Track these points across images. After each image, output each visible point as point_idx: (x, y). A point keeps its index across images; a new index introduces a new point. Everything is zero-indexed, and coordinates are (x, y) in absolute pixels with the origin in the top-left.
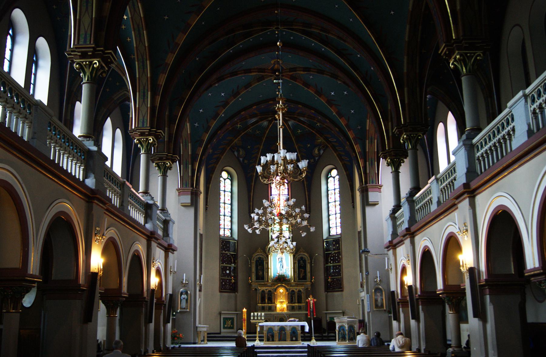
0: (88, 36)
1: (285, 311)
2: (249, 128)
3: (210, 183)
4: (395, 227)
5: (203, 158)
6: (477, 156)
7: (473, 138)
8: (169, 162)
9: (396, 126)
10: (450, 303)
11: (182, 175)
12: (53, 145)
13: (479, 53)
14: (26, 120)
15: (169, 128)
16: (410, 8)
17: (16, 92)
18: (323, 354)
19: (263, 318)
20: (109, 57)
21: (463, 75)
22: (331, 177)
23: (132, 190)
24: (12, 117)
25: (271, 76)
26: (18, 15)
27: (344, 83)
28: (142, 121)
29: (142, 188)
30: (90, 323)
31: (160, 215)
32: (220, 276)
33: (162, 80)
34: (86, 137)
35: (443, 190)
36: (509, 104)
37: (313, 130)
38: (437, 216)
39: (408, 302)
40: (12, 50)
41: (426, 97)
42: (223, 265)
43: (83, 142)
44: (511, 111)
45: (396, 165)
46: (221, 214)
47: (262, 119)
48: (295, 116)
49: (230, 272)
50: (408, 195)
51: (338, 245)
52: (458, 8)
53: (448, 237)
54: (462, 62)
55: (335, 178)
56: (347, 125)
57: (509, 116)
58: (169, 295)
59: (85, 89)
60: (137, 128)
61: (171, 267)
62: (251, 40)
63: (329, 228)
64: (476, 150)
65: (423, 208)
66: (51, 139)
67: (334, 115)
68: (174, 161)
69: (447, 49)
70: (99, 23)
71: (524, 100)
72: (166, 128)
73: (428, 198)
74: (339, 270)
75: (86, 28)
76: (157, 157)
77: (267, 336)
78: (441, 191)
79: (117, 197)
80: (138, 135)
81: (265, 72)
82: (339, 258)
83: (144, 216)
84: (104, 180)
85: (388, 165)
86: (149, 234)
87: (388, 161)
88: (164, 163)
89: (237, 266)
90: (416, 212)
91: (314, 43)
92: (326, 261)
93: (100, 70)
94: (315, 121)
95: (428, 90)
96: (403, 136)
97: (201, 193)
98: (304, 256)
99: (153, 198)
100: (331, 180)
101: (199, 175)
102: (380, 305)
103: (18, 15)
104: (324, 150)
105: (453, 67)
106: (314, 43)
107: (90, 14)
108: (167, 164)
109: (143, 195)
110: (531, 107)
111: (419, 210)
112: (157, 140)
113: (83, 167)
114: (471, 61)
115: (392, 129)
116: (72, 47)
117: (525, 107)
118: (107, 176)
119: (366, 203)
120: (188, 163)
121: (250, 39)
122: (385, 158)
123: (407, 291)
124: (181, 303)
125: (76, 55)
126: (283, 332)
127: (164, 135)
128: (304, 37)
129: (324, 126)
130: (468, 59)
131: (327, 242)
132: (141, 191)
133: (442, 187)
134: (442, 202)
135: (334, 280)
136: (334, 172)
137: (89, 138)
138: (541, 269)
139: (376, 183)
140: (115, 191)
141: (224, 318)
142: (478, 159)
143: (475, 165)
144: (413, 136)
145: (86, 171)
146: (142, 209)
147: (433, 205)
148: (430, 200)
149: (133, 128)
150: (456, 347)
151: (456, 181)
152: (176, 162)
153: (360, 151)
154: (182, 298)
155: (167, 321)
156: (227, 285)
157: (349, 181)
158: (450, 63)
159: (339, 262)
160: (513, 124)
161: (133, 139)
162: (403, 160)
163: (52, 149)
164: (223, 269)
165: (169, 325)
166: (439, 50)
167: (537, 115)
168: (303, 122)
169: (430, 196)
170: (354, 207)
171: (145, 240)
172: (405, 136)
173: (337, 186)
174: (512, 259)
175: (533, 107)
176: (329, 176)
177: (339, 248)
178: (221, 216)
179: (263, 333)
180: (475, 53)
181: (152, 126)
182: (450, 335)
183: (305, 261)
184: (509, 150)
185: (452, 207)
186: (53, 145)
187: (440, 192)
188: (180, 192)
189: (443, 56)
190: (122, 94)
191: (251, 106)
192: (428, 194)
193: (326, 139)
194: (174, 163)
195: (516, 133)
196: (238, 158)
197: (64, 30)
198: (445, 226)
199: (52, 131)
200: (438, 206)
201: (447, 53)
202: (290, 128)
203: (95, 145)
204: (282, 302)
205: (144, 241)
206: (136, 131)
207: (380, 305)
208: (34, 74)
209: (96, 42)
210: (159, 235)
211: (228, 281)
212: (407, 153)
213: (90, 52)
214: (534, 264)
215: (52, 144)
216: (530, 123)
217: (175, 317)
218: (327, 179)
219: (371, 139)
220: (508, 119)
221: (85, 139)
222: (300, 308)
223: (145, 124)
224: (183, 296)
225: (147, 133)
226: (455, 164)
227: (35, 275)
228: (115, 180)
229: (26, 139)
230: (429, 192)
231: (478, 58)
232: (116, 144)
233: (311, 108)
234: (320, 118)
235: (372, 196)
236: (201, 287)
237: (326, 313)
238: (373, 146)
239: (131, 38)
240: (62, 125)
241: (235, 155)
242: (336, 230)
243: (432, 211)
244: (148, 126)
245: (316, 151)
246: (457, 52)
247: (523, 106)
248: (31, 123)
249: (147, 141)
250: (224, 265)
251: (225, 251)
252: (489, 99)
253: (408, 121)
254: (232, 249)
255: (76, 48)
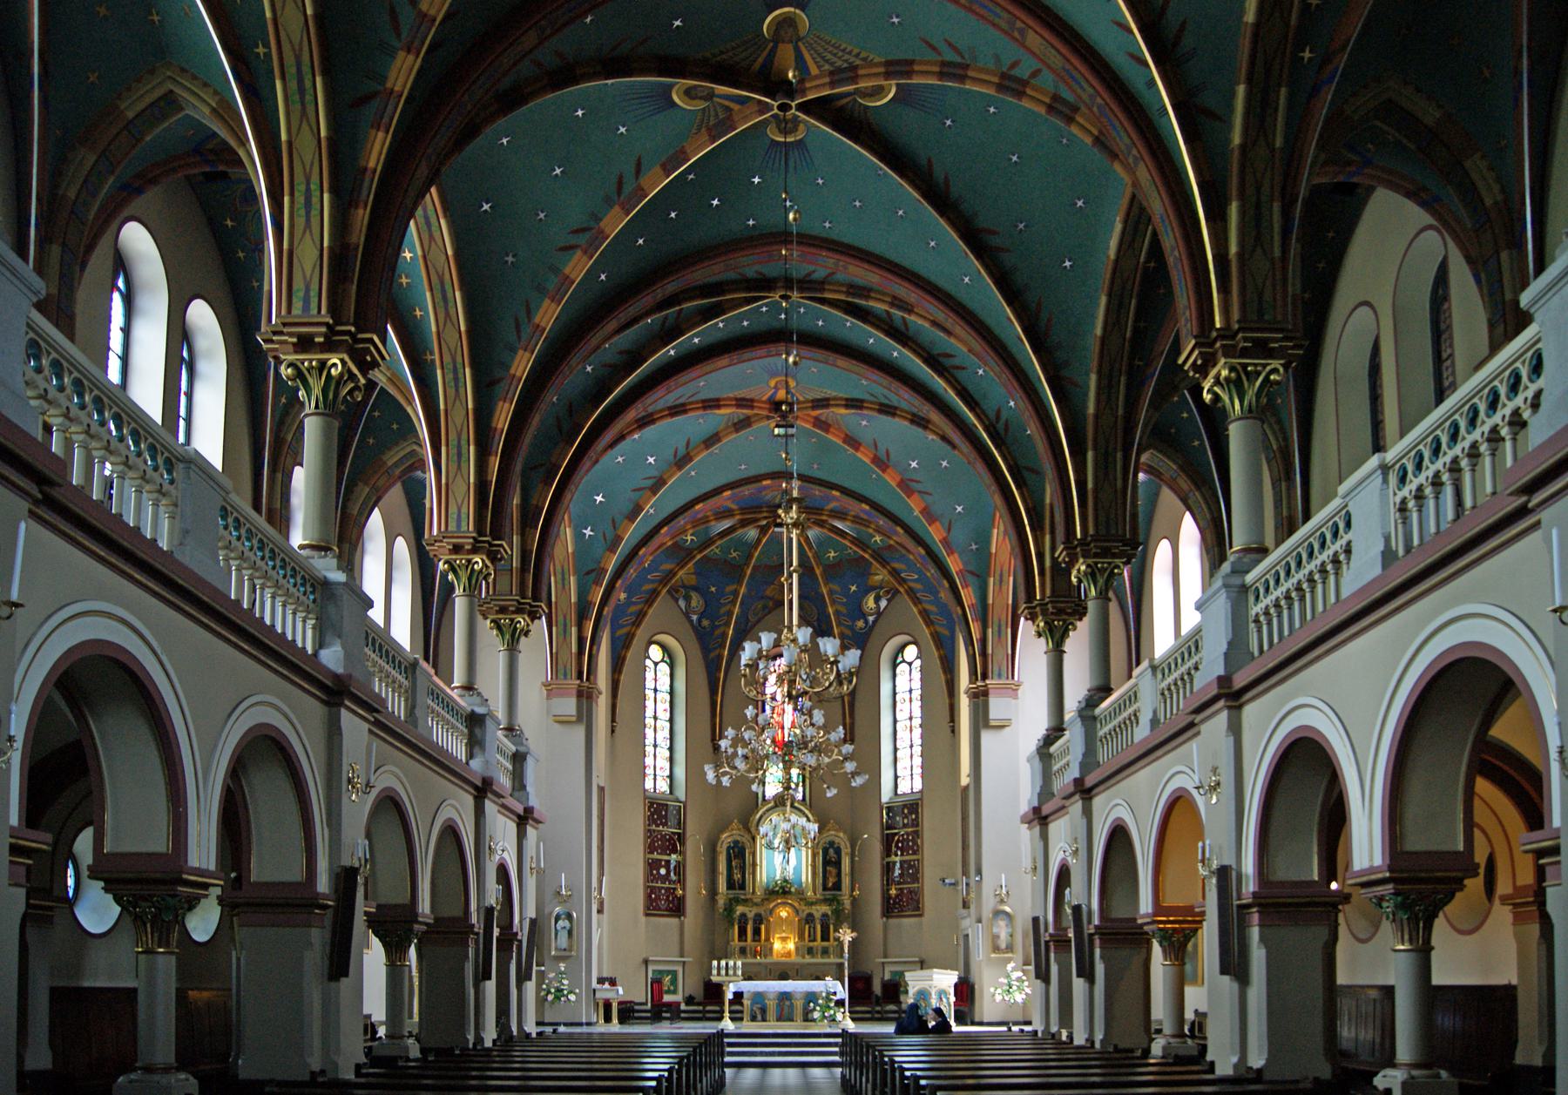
0: (314, 293)
1: (794, 958)
2: (714, 542)
3: (620, 672)
4: (1047, 776)
5: (605, 613)
6: (1253, 613)
7: (1247, 572)
8: (524, 619)
9: (1063, 543)
10: (1165, 944)
11: (554, 651)
12: (234, 564)
13: (1276, 364)
14: (161, 497)
15: (523, 534)
16: (1112, 253)
17: (51, 357)
18: (879, 1051)
19: (739, 972)
20: (368, 351)
21: (1233, 418)
22: (904, 661)
23: (436, 679)
24: (126, 489)
25: (768, 418)
26: (137, 238)
27: (944, 438)
28: (455, 516)
29: (458, 678)
30: (343, 980)
31: (505, 740)
32: (647, 880)
33: (503, 417)
34: (320, 548)
35: (1166, 692)
36: (1342, 489)
37: (864, 551)
38: (1149, 752)
39: (1070, 941)
40: (127, 330)
41: (1135, 476)
42: (651, 856)
43: (311, 561)
44: (1346, 506)
45: (1057, 636)
46: (647, 742)
47: (744, 523)
48: (824, 518)
49: (668, 872)
50: (1083, 705)
51: (914, 816)
52: (1233, 249)
53: (1170, 801)
54: (1232, 387)
55: (913, 666)
56: (945, 542)
57: (1340, 518)
58: (528, 920)
59: (312, 427)
60: (444, 535)
61: (532, 858)
62: (721, 325)
63: (896, 777)
64: (1252, 598)
65: (1117, 734)
66: (228, 547)
67: (916, 517)
68: (534, 616)
69: (1200, 353)
70: (339, 259)
71: (1381, 477)
72: (515, 537)
73: (1130, 710)
74: (913, 872)
75: (308, 274)
76: (495, 605)
77: (752, 1010)
78: (1163, 694)
79: (399, 696)
80: (447, 552)
81: (752, 407)
82: (915, 843)
83: (465, 741)
84: (366, 654)
85: (1039, 635)
86: (479, 783)
87: (1038, 626)
88: (512, 620)
89: (684, 860)
90: (1099, 743)
91: (874, 339)
92: (887, 852)
93: (346, 382)
94: (871, 531)
95: (1144, 458)
96: (1077, 567)
97: (600, 693)
98: (837, 840)
99: (487, 700)
100: (902, 668)
101: (594, 652)
102: (1003, 946)
103: (137, 238)
104: (889, 601)
105: (1211, 399)
106: (874, 339)
107: (466, 477)
108: (520, 622)
109: (464, 692)
110: (1395, 494)
111: (1106, 737)
112: (492, 563)
113: (313, 622)
114: (1254, 385)
115: (1053, 549)
116: (274, 322)
117: (1381, 494)
118: (373, 644)
119: (981, 720)
120: (568, 621)
121: (717, 323)
122: (1032, 617)
123: (1070, 917)
124: (556, 938)
125: (285, 342)
126: (787, 1003)
127: (510, 552)
128: (850, 321)
129: (892, 542)
130: (1248, 380)
131: (889, 809)
132: (456, 684)
133: (1164, 684)
134: (1162, 721)
135: (902, 892)
136: (911, 652)
137: (326, 551)
138: (1386, 868)
139: (1008, 678)
140: (394, 682)
141: (654, 971)
142: (1257, 621)
143: (1248, 633)
144: (1103, 567)
145: (321, 631)
146: (459, 725)
147: (1351, 571)
148: (1135, 715)
149: (435, 532)
150: (1174, 1036)
151: (1198, 673)
152: (540, 618)
153: (974, 602)
154: (558, 928)
155: (523, 976)
156: (661, 900)
157: (945, 672)
158: (1203, 388)
159: (915, 853)
160: (1346, 538)
161: (436, 560)
162: (1072, 624)
163: (246, 582)
164: (652, 866)
165: (530, 987)
166: (1179, 354)
167: (1408, 513)
168: (842, 533)
169: (1135, 707)
170: (953, 731)
171: (514, 825)
172: (1083, 568)
173: (917, 684)
174: (1315, 849)
175: (1400, 495)
176: (898, 661)
177: (915, 823)
178: (647, 748)
179: (742, 1004)
180: (1264, 366)
181: (480, 529)
182: (1160, 1010)
183: (838, 851)
184: (1332, 599)
185: (1188, 729)
186: (234, 564)
187: (1160, 697)
188: (551, 690)
189: (1187, 372)
190: (408, 450)
191: (717, 491)
192: (1130, 701)
193: (895, 573)
194: (536, 621)
195: (1353, 557)
196: (687, 615)
197: (256, 284)
198: (1164, 776)
199: (243, 538)
200: (1152, 729)
201: (1199, 362)
202: (811, 547)
203: (339, 568)
204: (784, 939)
205: (469, 800)
206: (441, 541)
207: (1003, 946)
208: (185, 394)
209: (334, 309)
210: (502, 786)
211: (663, 891)
212: (1086, 608)
213: (319, 335)
214: (1371, 859)
215: (232, 562)
216: (1390, 533)
217: (543, 968)
218: (894, 666)
219: (1001, 576)
220: (1336, 525)
221: (315, 553)
222: (825, 952)
223: (464, 524)
224: (561, 923)
225: (512, 609)
226: (1201, 631)
227: (207, 870)
228: (394, 656)
229: (164, 544)
230: (1133, 697)
231: (1272, 377)
232: (395, 575)
233: (861, 498)
234: (881, 523)
235: (997, 707)
236: (601, 903)
237: (883, 963)
238: (1003, 590)
239: (424, 308)
240: (261, 521)
241: (681, 609)
242: (911, 783)
243: (1136, 741)
244: (471, 528)
245: (871, 603)
246: (1223, 361)
247: (1378, 491)
248: (176, 505)
249: (470, 567)
250: (655, 856)
251: (658, 826)
252: (1284, 484)
253: (1091, 531)
254: (672, 821)
255: (285, 325)
